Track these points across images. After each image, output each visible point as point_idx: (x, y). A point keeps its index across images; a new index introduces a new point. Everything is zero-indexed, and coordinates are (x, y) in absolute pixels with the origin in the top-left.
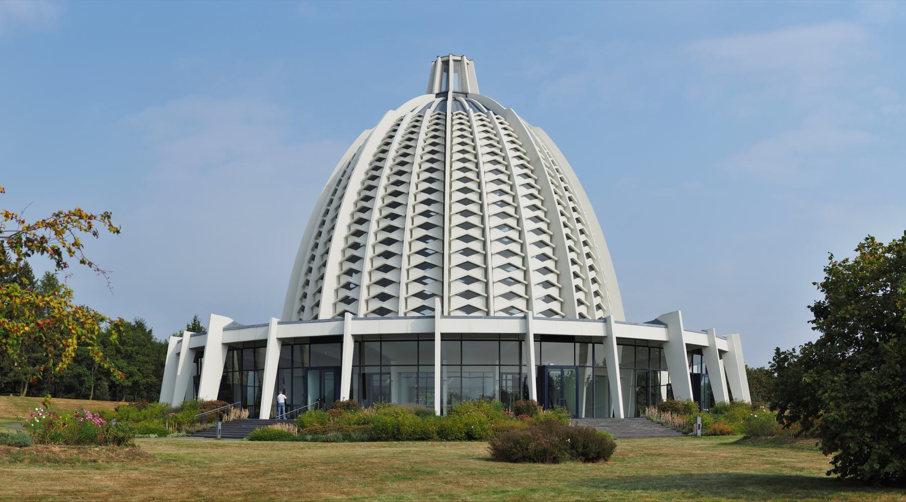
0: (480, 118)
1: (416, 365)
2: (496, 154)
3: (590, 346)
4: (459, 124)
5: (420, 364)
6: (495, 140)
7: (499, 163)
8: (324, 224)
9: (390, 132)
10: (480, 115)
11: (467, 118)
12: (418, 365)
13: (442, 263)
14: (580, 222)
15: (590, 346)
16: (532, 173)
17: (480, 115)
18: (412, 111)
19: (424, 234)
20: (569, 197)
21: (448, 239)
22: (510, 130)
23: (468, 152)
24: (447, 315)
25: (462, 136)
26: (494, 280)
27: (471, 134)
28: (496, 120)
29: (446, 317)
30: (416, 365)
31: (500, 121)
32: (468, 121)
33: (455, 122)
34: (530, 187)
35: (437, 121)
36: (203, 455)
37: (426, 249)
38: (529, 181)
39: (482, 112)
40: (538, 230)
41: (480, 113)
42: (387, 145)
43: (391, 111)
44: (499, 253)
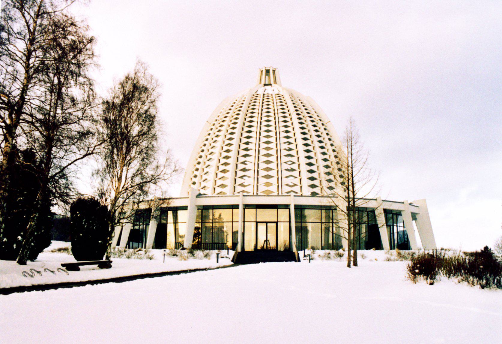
12: (233, 222)
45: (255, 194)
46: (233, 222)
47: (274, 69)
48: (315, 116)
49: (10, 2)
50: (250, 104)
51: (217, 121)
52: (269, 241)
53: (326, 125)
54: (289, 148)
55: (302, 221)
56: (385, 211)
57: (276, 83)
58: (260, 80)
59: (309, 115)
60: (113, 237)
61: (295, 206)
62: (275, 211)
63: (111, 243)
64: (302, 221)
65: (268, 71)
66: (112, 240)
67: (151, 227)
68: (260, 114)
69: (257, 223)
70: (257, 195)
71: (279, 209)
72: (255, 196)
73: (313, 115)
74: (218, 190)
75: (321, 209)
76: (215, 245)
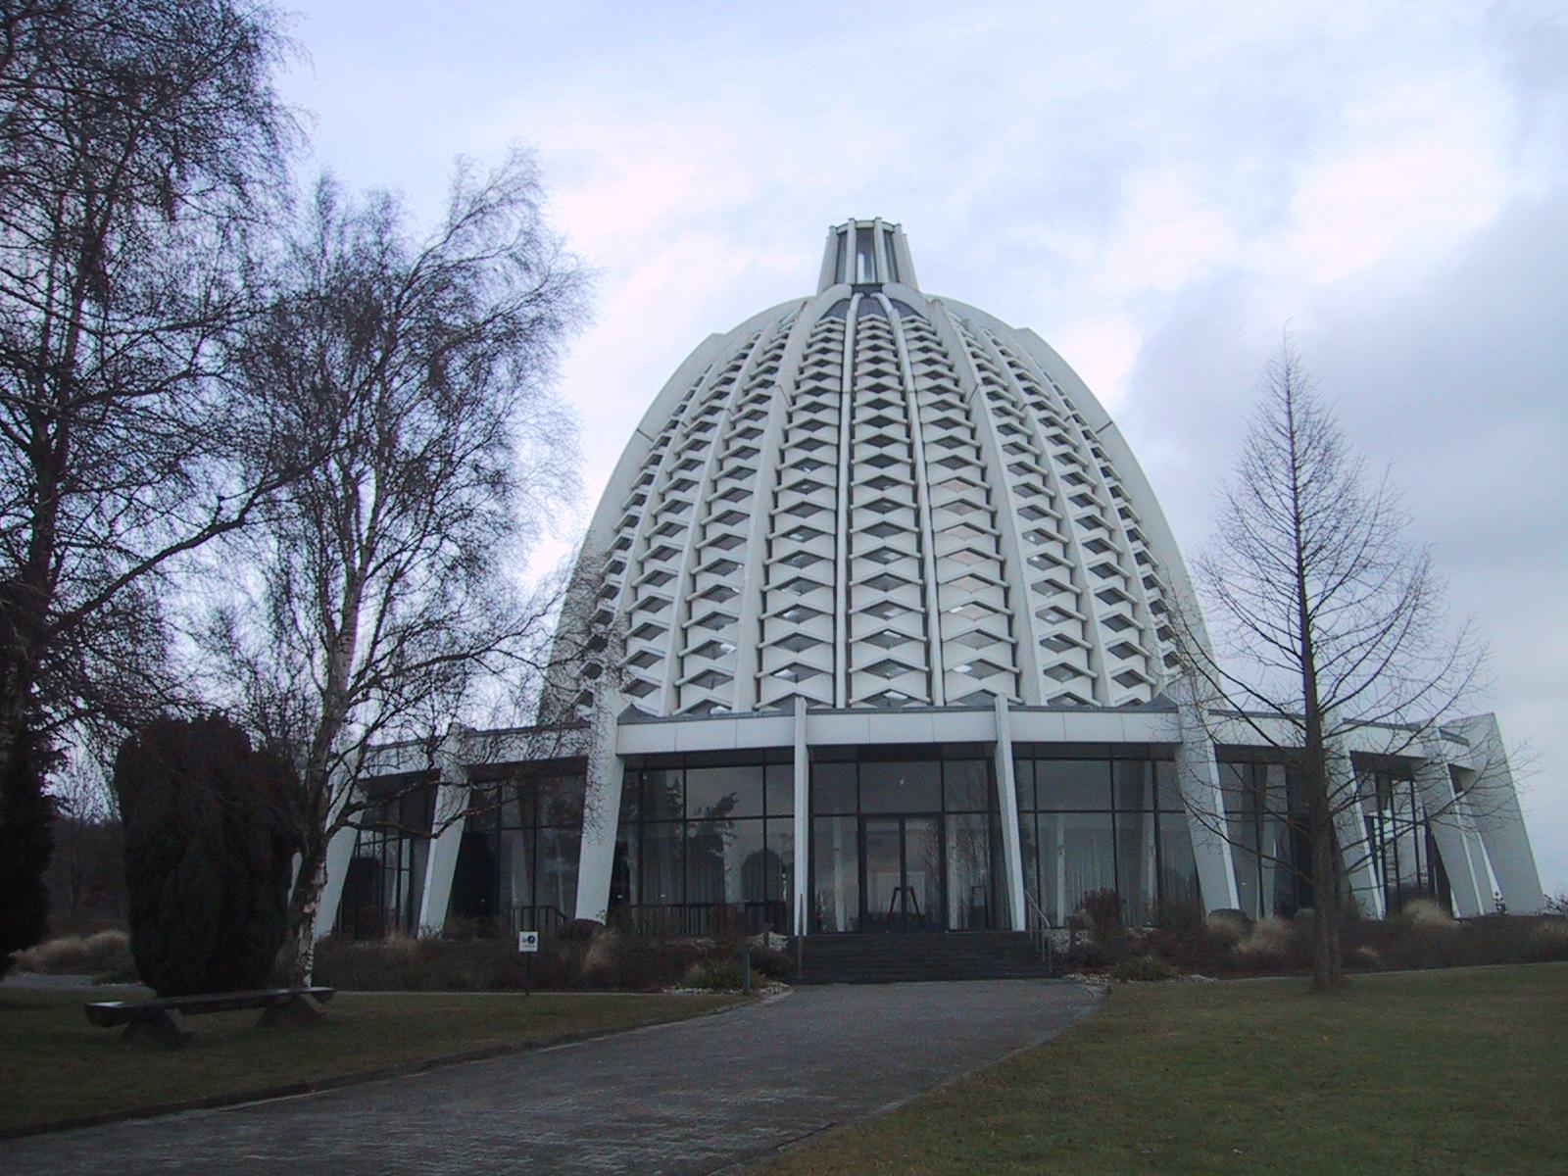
0: (913, 325)
1: (765, 822)
3: (1148, 765)
5: (768, 814)
6: (932, 341)
8: (682, 411)
9: (736, 359)
10: (913, 321)
12: (765, 817)
13: (833, 525)
14: (1109, 475)
15: (1148, 765)
16: (1021, 423)
17: (913, 321)
20: (1129, 532)
25: (876, 360)
26: (927, 459)
30: (765, 822)
32: (889, 332)
33: (862, 356)
34: (1030, 492)
36: (488, 750)
37: (803, 541)
38: (1028, 478)
39: (918, 315)
40: (1046, 585)
41: (914, 317)
43: (725, 332)
44: (938, 442)
45: (841, 705)
46: (765, 817)
47: (890, 229)
48: (1056, 403)
49: (2, 141)
50: (802, 372)
51: (679, 426)
52: (912, 890)
53: (1097, 437)
54: (887, 618)
55: (1117, 815)
56: (1226, 754)
57: (898, 281)
58: (837, 272)
59: (1035, 399)
60: (321, 886)
61: (1016, 746)
62: (933, 767)
63: (313, 913)
64: (1117, 815)
65: (865, 234)
66: (314, 899)
67: (435, 858)
68: (846, 398)
69: (863, 819)
70: (849, 709)
71: (947, 764)
72: (841, 712)
73: (1047, 398)
74: (693, 696)
75: (1111, 759)
76: (703, 910)
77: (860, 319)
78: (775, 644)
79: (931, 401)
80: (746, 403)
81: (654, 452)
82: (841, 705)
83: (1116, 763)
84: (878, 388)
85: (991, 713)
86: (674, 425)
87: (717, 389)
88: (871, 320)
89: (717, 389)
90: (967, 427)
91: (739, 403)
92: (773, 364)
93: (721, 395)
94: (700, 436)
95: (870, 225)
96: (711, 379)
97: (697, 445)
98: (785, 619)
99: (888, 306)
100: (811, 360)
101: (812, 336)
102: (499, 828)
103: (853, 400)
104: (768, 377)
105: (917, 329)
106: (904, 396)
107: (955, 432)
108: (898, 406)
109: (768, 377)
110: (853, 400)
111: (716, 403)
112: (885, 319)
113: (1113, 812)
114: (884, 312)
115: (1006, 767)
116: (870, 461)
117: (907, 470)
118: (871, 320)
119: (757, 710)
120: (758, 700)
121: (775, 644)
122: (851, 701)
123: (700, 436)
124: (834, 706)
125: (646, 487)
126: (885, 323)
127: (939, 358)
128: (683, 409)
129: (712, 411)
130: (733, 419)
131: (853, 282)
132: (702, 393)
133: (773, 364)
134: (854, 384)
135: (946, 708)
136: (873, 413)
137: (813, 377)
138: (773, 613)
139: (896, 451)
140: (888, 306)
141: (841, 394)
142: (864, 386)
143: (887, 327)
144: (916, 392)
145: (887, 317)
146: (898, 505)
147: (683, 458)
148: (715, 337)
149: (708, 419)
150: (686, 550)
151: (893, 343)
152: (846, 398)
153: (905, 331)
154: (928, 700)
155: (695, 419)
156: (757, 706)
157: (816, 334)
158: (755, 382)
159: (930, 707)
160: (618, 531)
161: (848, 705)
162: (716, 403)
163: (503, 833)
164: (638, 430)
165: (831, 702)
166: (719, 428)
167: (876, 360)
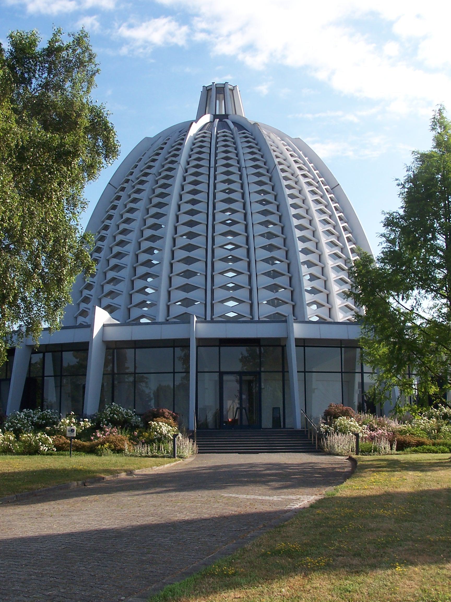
2: (253, 147)
4: (223, 152)
7: (258, 160)
10: (244, 133)
11: (232, 136)
17: (244, 133)
18: (180, 132)
19: (190, 208)
21: (210, 288)
22: (310, 178)
23: (231, 158)
24: (210, 320)
25: (227, 158)
27: (234, 143)
28: (305, 186)
29: (209, 322)
31: (307, 180)
32: (233, 138)
33: (220, 144)
35: (204, 134)
42: (158, 155)
43: (152, 137)
45: (209, 318)
51: (130, 182)
68: (212, 170)
77: (218, 132)
78: (178, 261)
79: (248, 151)
80: (165, 164)
81: (117, 194)
82: (209, 318)
83: (343, 349)
84: (228, 173)
85: (284, 324)
86: (127, 181)
87: (152, 157)
88: (224, 132)
89: (152, 157)
90: (284, 249)
91: (163, 164)
92: (179, 147)
93: (150, 167)
94: (140, 187)
95: (223, 86)
96: (145, 159)
97: (139, 191)
98: (180, 276)
99: (232, 126)
100: (195, 151)
101: (195, 140)
102: (43, 376)
103: (215, 171)
104: (173, 159)
105: (246, 137)
106: (238, 162)
107: (268, 207)
108: (237, 174)
109: (173, 159)
110: (215, 171)
111: (148, 171)
112: (231, 132)
113: (342, 372)
114: (230, 129)
115: (295, 386)
116: (224, 182)
117: (240, 195)
118: (224, 132)
119: (168, 320)
120: (168, 315)
121: (178, 261)
122: (213, 317)
123: (140, 187)
124: (205, 319)
125: (122, 192)
126: (231, 134)
127: (254, 145)
128: (136, 166)
129: (146, 175)
130: (157, 179)
131: (214, 114)
132: (141, 166)
133: (179, 147)
134: (216, 163)
135: (259, 322)
136: (225, 169)
137: (197, 153)
138: (179, 247)
139: (237, 206)
140: (232, 126)
141: (209, 168)
142: (221, 164)
143: (232, 136)
144: (246, 168)
145: (231, 130)
146: (231, 158)
147: (136, 188)
148: (147, 138)
149: (144, 178)
150: (144, 200)
151: (234, 143)
152: (212, 170)
153: (241, 142)
154: (251, 317)
155: (138, 178)
156: (168, 318)
157: (197, 139)
158: (170, 155)
159: (252, 321)
160: (103, 222)
161: (212, 319)
162: (148, 171)
163: (45, 378)
164: (109, 183)
165: (204, 318)
166: (150, 183)
167: (227, 158)
